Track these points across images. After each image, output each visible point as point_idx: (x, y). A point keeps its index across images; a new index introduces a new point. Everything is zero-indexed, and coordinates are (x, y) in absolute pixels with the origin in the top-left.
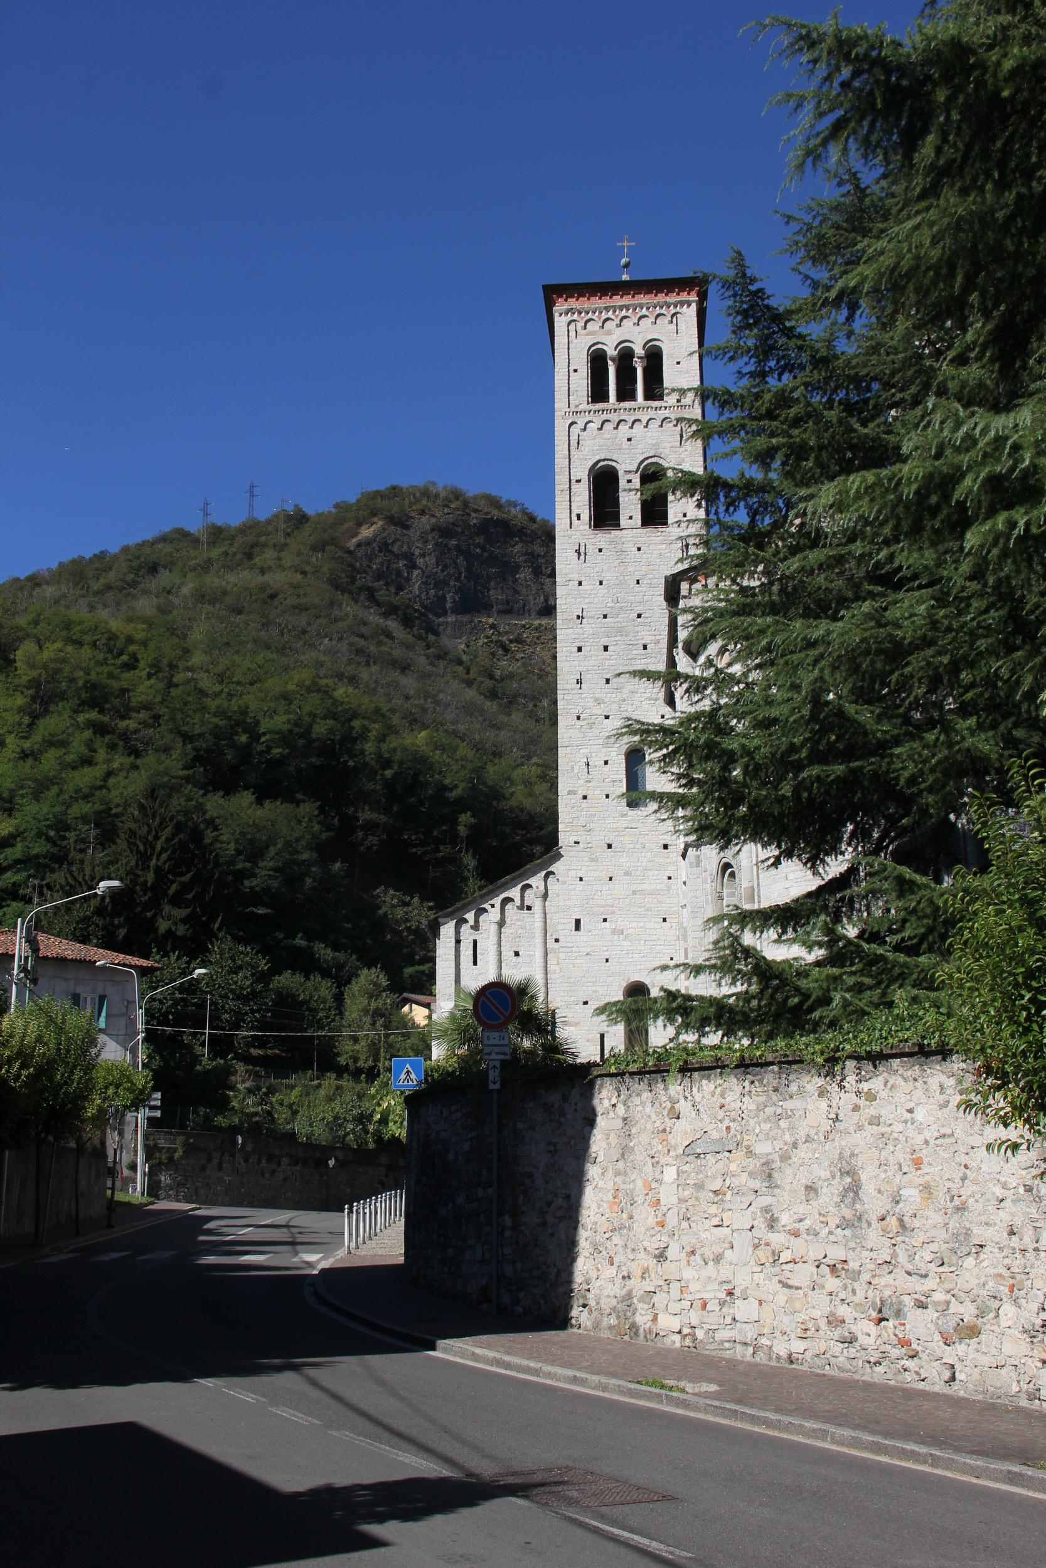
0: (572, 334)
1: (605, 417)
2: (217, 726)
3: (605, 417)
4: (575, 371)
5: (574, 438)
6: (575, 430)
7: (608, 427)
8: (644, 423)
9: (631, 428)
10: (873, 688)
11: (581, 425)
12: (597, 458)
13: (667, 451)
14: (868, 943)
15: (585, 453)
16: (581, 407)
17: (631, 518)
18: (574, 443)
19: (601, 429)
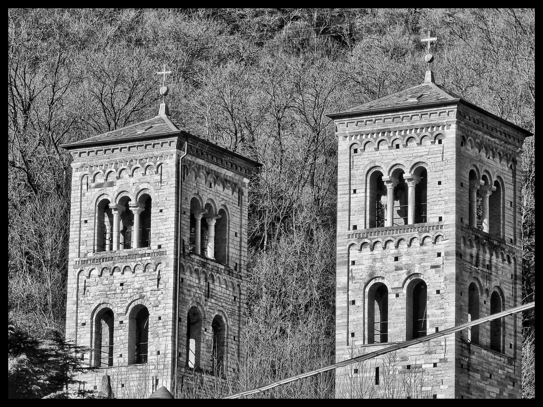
0: (85, 187)
1: (104, 265)
2: (526, 313)
3: (104, 265)
4: (86, 222)
5: (82, 285)
6: (83, 277)
7: (107, 274)
8: (132, 268)
9: (123, 273)
10: (124, 235)
11: (86, 273)
12: (98, 302)
13: (148, 294)
14: (167, 113)
15: (90, 298)
16: (90, 255)
17: (121, 356)
18: (81, 288)
19: (100, 276)
